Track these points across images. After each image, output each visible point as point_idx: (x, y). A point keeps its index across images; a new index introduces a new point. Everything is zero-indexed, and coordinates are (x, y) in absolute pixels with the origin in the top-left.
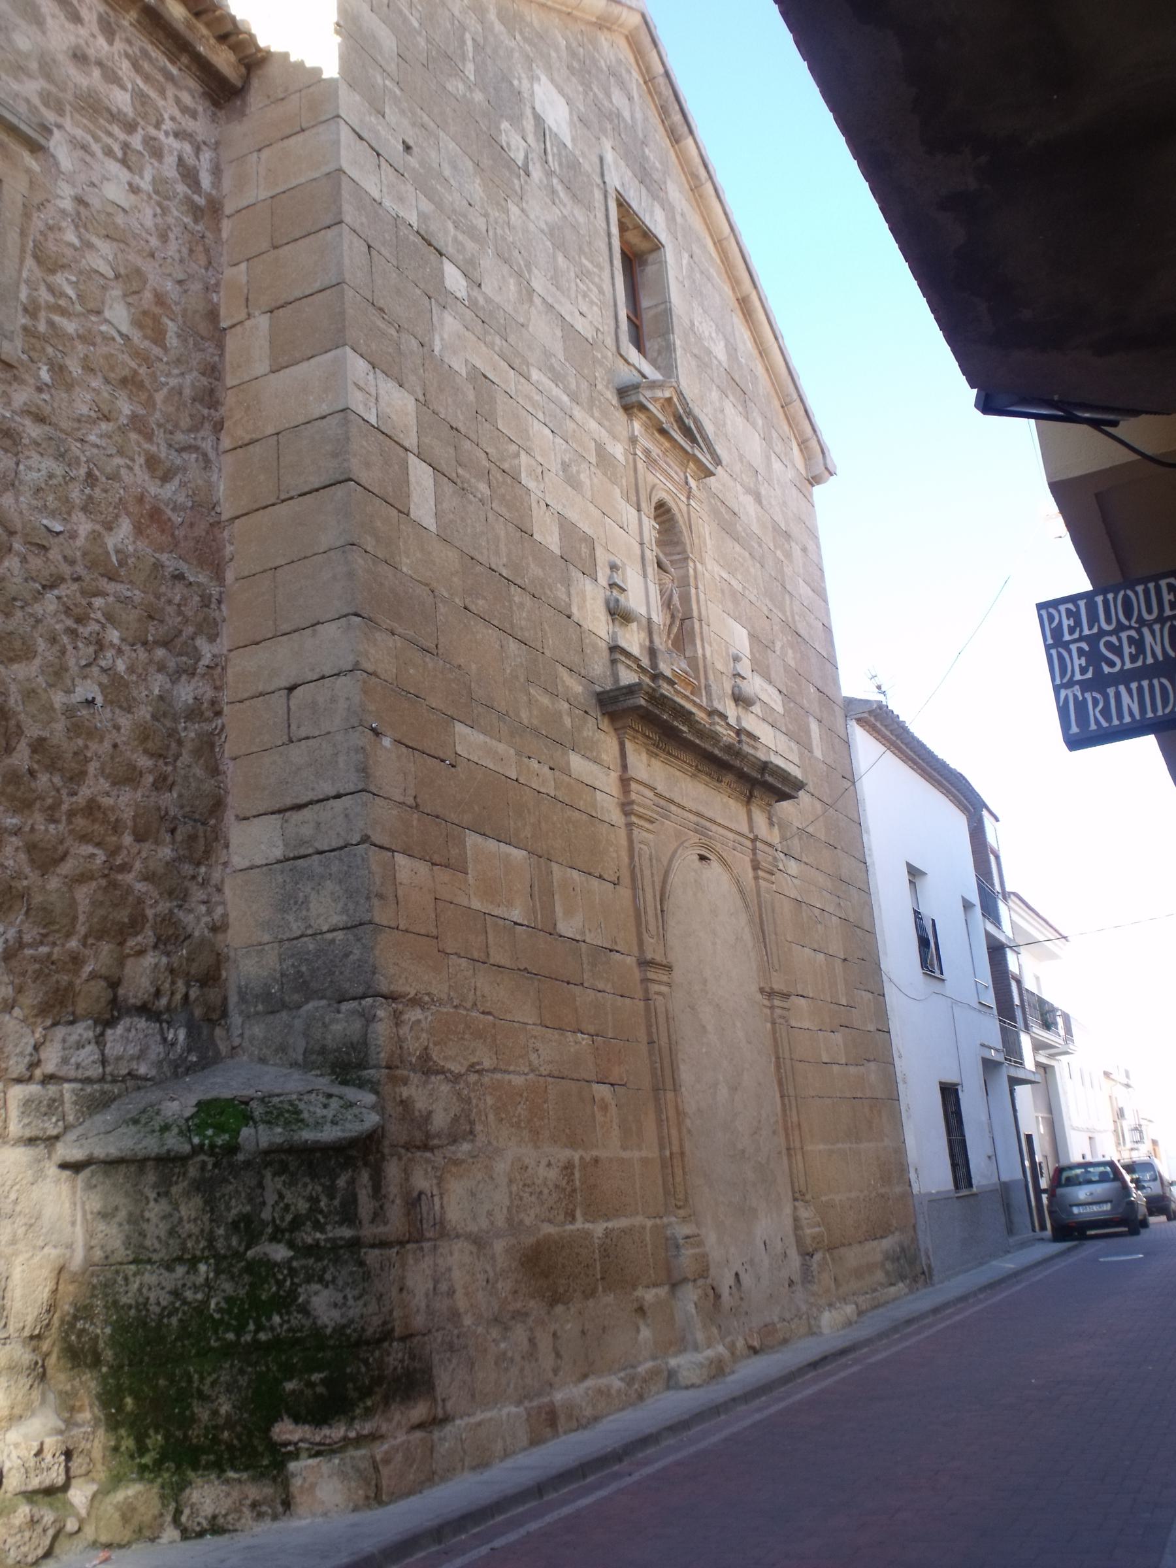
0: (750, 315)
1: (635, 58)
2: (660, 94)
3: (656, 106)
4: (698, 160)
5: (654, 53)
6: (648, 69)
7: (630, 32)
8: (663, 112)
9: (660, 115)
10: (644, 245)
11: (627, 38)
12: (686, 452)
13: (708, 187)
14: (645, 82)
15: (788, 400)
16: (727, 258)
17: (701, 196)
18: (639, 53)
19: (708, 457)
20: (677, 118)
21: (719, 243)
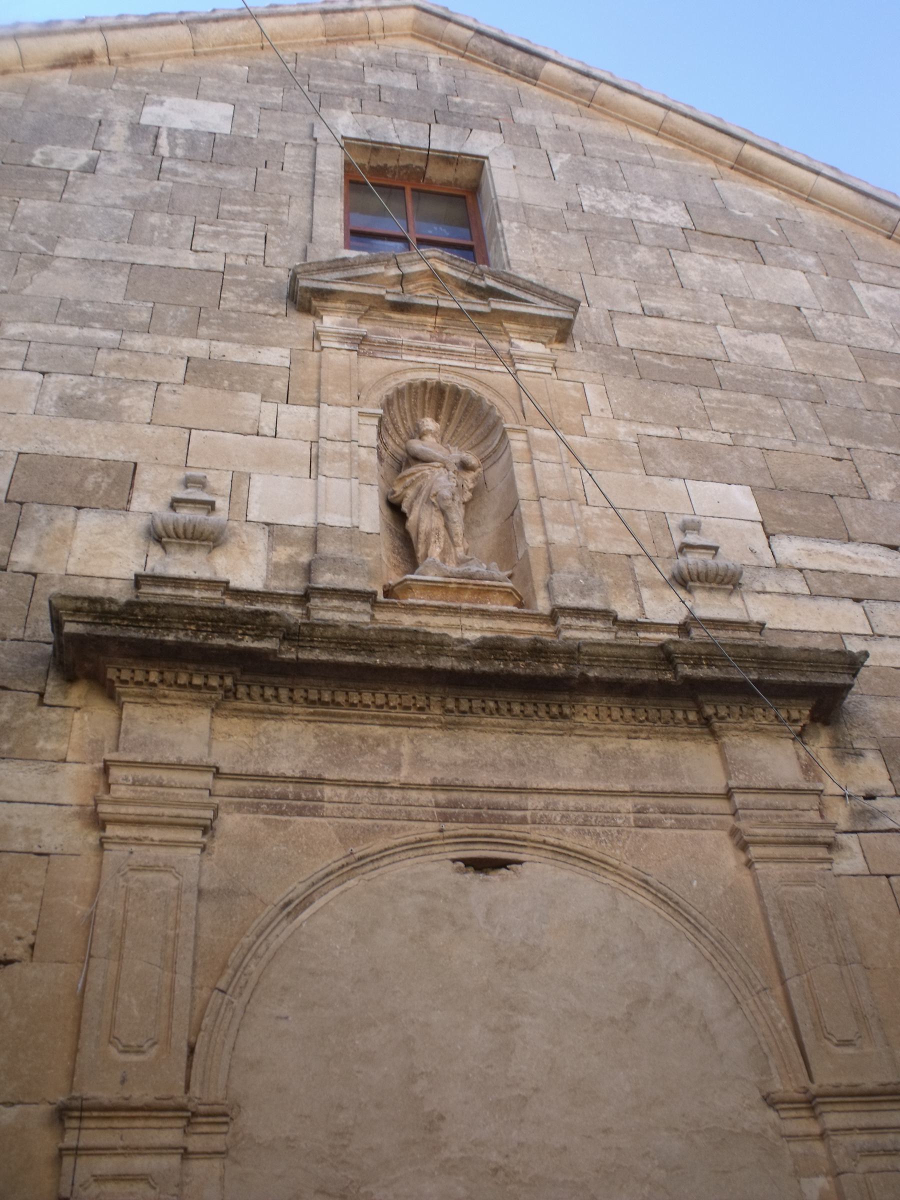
0: (761, 173)
1: (435, 44)
2: (483, 54)
3: (488, 66)
4: (569, 76)
5: (451, 27)
6: (455, 43)
7: (413, 29)
8: (501, 65)
9: (499, 70)
10: (465, 173)
11: (413, 36)
12: (480, 314)
13: (606, 91)
14: (463, 56)
15: (889, 225)
16: (682, 137)
17: (602, 104)
18: (435, 38)
19: (543, 304)
20: (518, 58)
21: (660, 130)
